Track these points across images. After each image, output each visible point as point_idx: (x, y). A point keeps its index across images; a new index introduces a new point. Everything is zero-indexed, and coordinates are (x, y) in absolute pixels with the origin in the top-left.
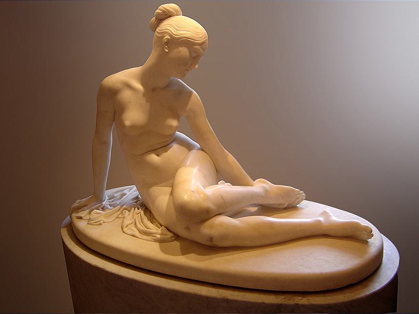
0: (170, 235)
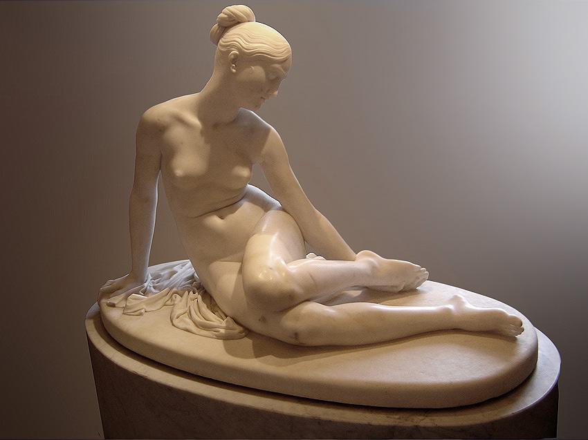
0: (238, 329)
